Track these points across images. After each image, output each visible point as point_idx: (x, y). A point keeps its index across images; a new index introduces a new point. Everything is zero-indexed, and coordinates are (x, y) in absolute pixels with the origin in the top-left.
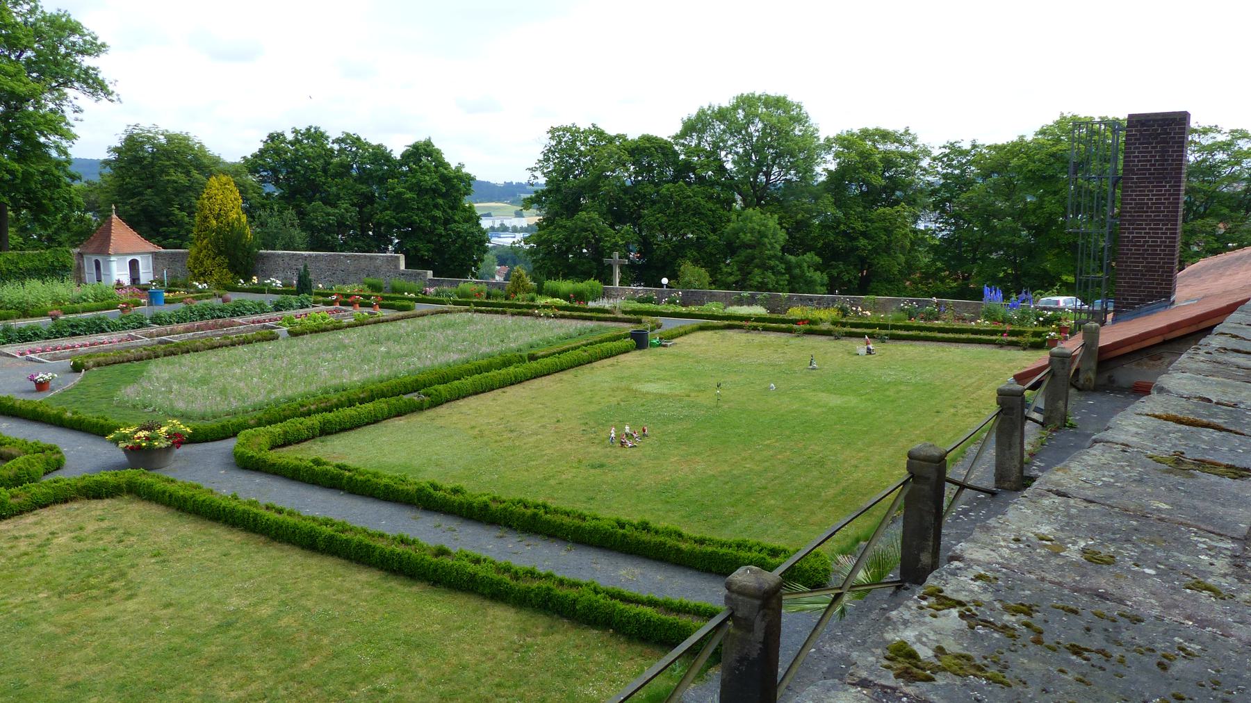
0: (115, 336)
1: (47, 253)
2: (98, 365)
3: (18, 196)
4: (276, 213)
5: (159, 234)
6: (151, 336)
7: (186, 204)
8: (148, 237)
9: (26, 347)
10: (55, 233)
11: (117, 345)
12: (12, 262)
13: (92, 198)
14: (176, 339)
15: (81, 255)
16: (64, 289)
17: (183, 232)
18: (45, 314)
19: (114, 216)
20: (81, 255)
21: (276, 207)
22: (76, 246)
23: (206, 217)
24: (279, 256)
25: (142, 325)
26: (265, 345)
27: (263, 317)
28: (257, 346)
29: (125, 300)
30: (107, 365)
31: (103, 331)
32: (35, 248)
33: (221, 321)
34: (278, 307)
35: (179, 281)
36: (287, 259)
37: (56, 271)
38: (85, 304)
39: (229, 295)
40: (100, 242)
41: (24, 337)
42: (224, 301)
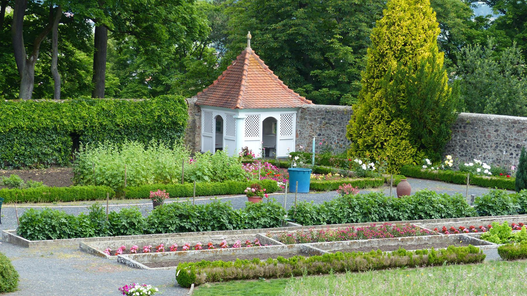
0: (239, 236)
1: (154, 103)
2: (213, 279)
3: (125, 15)
4: (489, 52)
5: (307, 78)
6: (288, 240)
7: (353, 34)
8: (293, 84)
9: (119, 242)
10: (163, 72)
11: (240, 251)
12: (107, 113)
13: (219, 21)
14: (326, 249)
15: (198, 107)
16: (169, 158)
17: (344, 78)
18: (144, 196)
19: (249, 49)
20: (198, 107)
21: (490, 42)
22: (193, 94)
23: (383, 56)
24: (490, 123)
25: (276, 222)
26: (463, 269)
27: (460, 223)
28: (451, 270)
29: (254, 181)
30: (227, 280)
31: (222, 227)
32: (136, 94)
33: (394, 224)
34: (484, 209)
35: (333, 155)
36: (502, 129)
37: (163, 130)
38: (198, 183)
39: (410, 184)
40: (217, 84)
41: (117, 228)
42: (400, 193)
